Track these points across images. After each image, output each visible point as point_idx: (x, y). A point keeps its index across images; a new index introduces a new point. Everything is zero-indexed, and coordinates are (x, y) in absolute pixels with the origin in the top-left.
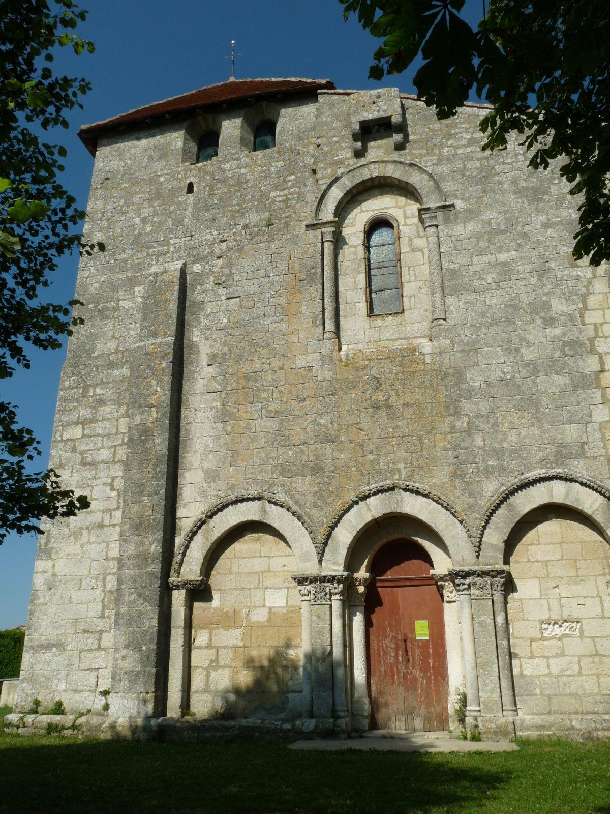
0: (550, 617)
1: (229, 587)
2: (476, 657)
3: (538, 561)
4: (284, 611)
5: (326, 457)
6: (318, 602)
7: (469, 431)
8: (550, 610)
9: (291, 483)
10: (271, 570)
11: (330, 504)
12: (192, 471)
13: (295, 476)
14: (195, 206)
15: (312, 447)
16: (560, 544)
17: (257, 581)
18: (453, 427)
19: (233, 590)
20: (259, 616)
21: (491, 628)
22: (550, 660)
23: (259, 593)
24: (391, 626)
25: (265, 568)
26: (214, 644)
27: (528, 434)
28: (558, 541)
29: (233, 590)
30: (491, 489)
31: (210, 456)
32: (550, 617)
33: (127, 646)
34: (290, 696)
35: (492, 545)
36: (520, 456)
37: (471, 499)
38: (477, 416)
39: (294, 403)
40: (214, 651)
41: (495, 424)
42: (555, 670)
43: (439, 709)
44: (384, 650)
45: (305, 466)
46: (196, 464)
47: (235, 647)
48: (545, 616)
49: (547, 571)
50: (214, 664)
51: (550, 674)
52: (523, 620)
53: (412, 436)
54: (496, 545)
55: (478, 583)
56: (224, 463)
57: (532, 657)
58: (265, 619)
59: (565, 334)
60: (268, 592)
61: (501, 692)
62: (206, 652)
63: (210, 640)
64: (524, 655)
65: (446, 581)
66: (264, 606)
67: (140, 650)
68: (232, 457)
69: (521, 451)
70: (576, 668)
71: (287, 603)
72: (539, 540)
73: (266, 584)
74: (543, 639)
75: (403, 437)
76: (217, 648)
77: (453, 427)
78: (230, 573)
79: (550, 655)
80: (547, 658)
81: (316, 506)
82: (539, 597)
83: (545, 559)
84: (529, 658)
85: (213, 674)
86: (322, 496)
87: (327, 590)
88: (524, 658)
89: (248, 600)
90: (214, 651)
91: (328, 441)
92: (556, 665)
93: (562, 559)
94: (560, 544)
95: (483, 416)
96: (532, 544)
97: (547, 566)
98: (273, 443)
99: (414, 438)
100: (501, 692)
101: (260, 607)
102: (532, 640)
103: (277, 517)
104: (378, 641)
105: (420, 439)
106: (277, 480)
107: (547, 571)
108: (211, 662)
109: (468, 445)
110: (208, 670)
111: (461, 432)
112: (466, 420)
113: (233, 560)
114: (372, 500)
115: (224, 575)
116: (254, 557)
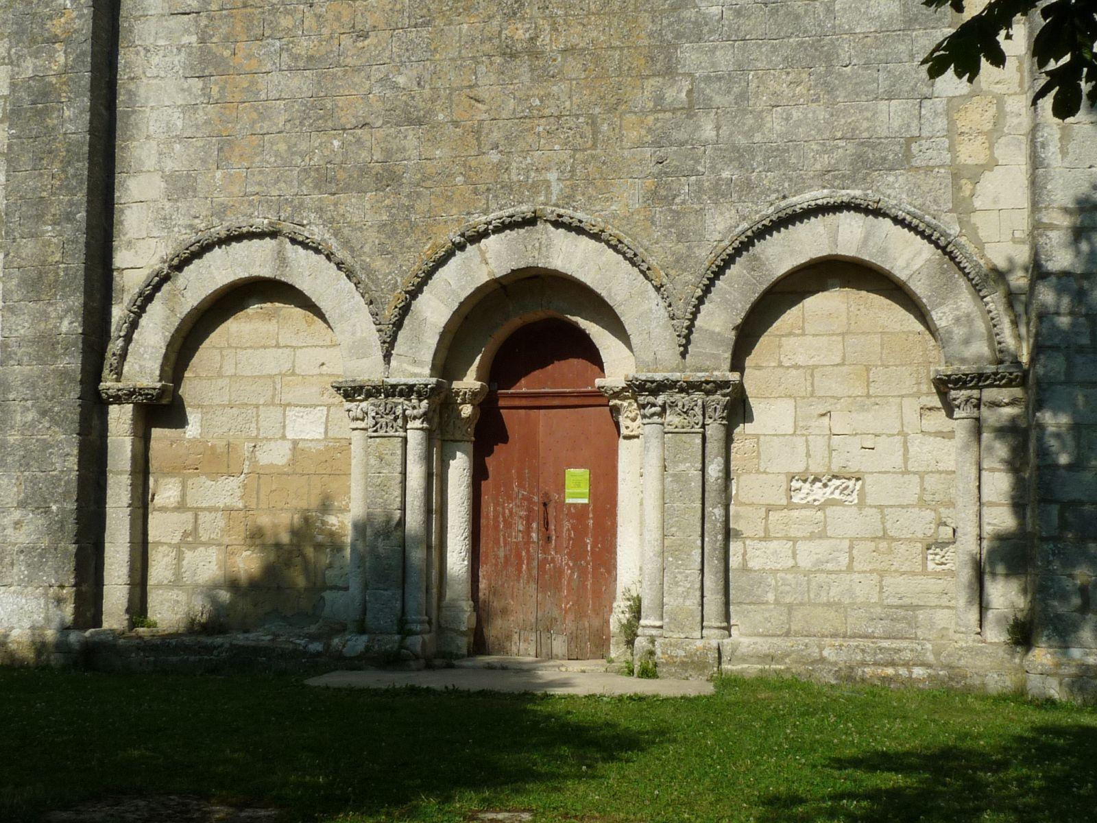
1: (217, 401)
6: (381, 433)
8: (808, 455)
9: (335, 205)
10: (297, 371)
15: (380, 133)
16: (843, 334)
17: (270, 393)
18: (659, 99)
19: (224, 406)
21: (696, 485)
23: (275, 413)
25: (286, 367)
32: (807, 469)
33: (22, 505)
37: (680, 246)
38: (708, 79)
39: (346, 41)
40: (189, 516)
41: (743, 96)
42: (805, 562)
44: (505, 521)
45: (364, 170)
47: (229, 510)
48: (799, 467)
49: (812, 385)
50: (190, 539)
52: (758, 471)
53: (577, 116)
54: (719, 334)
56: (204, 161)
57: (766, 538)
60: (291, 413)
62: (175, 516)
63: (183, 495)
66: (284, 437)
67: (47, 511)
70: (844, 560)
72: (803, 328)
73: (286, 398)
74: (790, 506)
75: (559, 117)
76: (196, 511)
77: (659, 99)
78: (220, 376)
79: (799, 535)
80: (794, 540)
81: (383, 251)
82: (791, 432)
84: (760, 540)
85: (188, 555)
86: (395, 232)
87: (399, 411)
88: (752, 539)
89: (254, 425)
90: (189, 516)
92: (808, 554)
93: (842, 364)
95: (720, 79)
96: (790, 334)
97: (812, 375)
99: (581, 120)
103: (305, 271)
104: (497, 504)
107: (812, 385)
108: (185, 534)
109: (686, 136)
111: (674, 111)
112: (686, 85)
115: (210, 378)
116: (265, 347)
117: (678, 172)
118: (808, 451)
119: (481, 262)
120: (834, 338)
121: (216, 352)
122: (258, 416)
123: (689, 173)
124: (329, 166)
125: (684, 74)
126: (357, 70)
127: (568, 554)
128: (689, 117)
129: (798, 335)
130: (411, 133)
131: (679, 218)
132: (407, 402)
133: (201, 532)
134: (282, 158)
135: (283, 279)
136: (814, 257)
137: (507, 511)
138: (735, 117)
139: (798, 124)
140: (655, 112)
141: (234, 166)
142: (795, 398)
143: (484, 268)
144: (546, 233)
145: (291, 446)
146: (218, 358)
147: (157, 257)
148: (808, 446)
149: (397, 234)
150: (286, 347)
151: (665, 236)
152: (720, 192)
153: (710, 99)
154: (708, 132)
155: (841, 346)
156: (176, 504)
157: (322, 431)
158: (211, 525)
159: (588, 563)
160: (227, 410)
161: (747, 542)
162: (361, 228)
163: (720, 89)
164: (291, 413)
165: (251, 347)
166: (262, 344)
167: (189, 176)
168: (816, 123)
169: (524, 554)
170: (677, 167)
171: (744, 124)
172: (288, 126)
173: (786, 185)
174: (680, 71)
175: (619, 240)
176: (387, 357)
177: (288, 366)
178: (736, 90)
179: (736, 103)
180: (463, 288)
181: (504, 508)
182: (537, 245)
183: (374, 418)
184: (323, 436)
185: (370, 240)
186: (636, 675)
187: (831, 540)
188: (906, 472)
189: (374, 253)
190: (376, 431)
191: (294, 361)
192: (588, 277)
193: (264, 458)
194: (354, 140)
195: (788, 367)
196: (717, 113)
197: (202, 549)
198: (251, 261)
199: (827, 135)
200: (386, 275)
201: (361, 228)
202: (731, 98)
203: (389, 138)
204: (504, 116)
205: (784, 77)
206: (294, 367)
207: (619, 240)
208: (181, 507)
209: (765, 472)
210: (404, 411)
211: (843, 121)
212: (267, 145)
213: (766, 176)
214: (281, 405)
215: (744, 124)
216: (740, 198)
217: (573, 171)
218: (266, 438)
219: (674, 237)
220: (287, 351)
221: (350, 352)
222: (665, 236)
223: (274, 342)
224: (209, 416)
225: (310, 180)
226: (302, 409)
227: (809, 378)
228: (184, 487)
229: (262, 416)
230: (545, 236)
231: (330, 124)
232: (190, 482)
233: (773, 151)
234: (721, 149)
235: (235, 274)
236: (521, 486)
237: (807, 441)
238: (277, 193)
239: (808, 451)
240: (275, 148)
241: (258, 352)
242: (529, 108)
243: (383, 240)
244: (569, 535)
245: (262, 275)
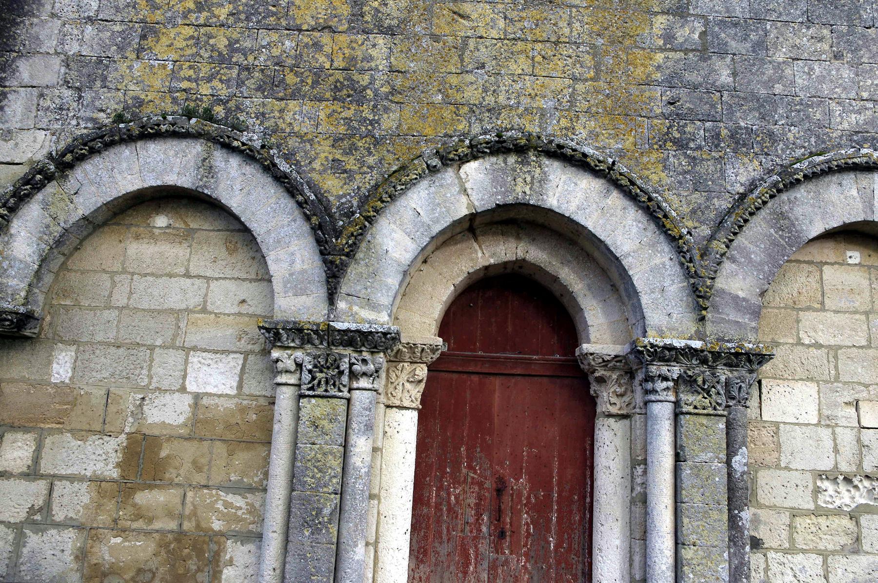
0: (836, 466)
1: (99, 337)
2: (293, 490)
3: (818, 346)
4: (231, 404)
5: (373, 64)
6: (320, 391)
7: (705, 49)
8: (836, 450)
9: (281, 111)
10: (210, 307)
11: (371, 168)
12: (37, 59)
13: (293, 97)
15: (343, 39)
16: (867, 313)
17: (170, 333)
18: (668, 37)
19: (108, 344)
22: (830, 560)
23: (174, 358)
24: (470, 459)
25: (194, 301)
26: (46, 467)
27: (829, 74)
28: (863, 308)
29: (108, 344)
30: (743, 179)
31: (89, 28)
32: (836, 466)
35: (736, 298)
36: (808, 117)
37: (697, 195)
38: (722, 24)
41: (760, 45)
44: (450, 510)
45: (318, 74)
46: (50, 45)
47: (97, 480)
48: (826, 464)
49: (836, 368)
50: (38, 517)
52: (778, 467)
53: (578, 45)
54: (744, 299)
55: (700, 380)
56: (121, 49)
57: (792, 550)
58: (181, 420)
60: (195, 359)
62: (23, 486)
63: (37, 459)
64: (774, 545)
65: (614, 369)
66: (183, 389)
68: (143, 37)
69: (811, 106)
71: (240, 386)
72: (822, 303)
73: (192, 339)
75: (557, 43)
76: (52, 479)
77: (668, 37)
78: (108, 307)
79: (830, 547)
81: (336, 166)
82: (815, 421)
83: (832, 342)
84: (786, 552)
85: (33, 540)
86: (353, 148)
87: (344, 366)
88: (776, 551)
89: (145, 372)
90: (41, 486)
93: (869, 346)
94: (867, 313)
95: (736, 25)
96: (809, 309)
97: (836, 357)
98: (248, 19)
99: (582, 48)
101: (174, 392)
102: (795, 513)
103: (239, 186)
104: (440, 488)
105: (595, 51)
106: (247, 102)
107: (836, 368)
108: (32, 511)
109: (700, 79)
111: (686, 51)
112: (699, 27)
113: (117, 278)
114: (473, 170)
115: (91, 308)
116: (170, 276)
117: (691, 116)
118: (836, 445)
119: (459, 192)
120: (857, 316)
121: (105, 276)
122: (152, 360)
123: (705, 118)
124: (277, 68)
125: (697, 15)
127: (526, 555)
128: (704, 59)
129: (816, 310)
130: (381, 42)
131: (695, 165)
132: (355, 355)
133: (56, 509)
134: (220, 54)
135: (206, 191)
136: (847, 221)
137: (453, 498)
138: (754, 65)
139: (821, 79)
140: (666, 50)
141: (159, 57)
142: (818, 382)
143: (464, 199)
144: (540, 166)
145: (191, 402)
146: (108, 284)
147: (45, 152)
148: (835, 440)
149: (356, 149)
150: (199, 277)
151: (680, 183)
152: (740, 142)
153: (726, 44)
154: (725, 77)
155: (865, 327)
156: (25, 469)
157: (235, 384)
159: (550, 567)
160: (112, 350)
161: (769, 555)
162: (312, 140)
163: (736, 35)
164: (195, 360)
165: (152, 274)
166: (168, 271)
167: (100, 61)
168: (840, 81)
169: (471, 551)
170: (689, 109)
171: (764, 74)
172: (231, 20)
173: (813, 140)
174: (691, 12)
175: (630, 181)
176: (331, 298)
177: (198, 300)
178: (753, 37)
179: (754, 51)
180: (436, 221)
181: (449, 494)
182: (529, 179)
183: (310, 371)
184: (234, 392)
185: (323, 155)
187: (868, 556)
189: (325, 171)
190: (312, 389)
191: (206, 295)
192: (591, 222)
194: (311, 43)
195: (809, 346)
196: (733, 59)
197: (53, 532)
198: (168, 164)
199: (853, 95)
200: (339, 197)
201: (312, 140)
202: (748, 45)
203: (354, 45)
204: (492, 35)
205: (804, 30)
206: (205, 302)
207: (630, 181)
208: (32, 473)
209: (787, 468)
210: (351, 365)
211: (869, 82)
212: (204, 39)
213: (790, 131)
214: (183, 348)
215: (764, 74)
216: (762, 150)
217: (572, 102)
218: (159, 389)
219: (690, 185)
220: (197, 282)
221: (285, 286)
222: (680, 183)
223: (182, 270)
224: (87, 356)
225: (253, 81)
226: (209, 355)
227: (831, 359)
229: (157, 360)
230: (538, 170)
231: (284, 23)
232: (48, 441)
233: (796, 105)
234: (738, 97)
235: (144, 181)
236: (470, 467)
237: (834, 433)
238: (210, 91)
239: (836, 445)
240: (212, 41)
241: (160, 280)
242: (522, 30)
243: (338, 157)
244: (528, 530)
245: (179, 184)
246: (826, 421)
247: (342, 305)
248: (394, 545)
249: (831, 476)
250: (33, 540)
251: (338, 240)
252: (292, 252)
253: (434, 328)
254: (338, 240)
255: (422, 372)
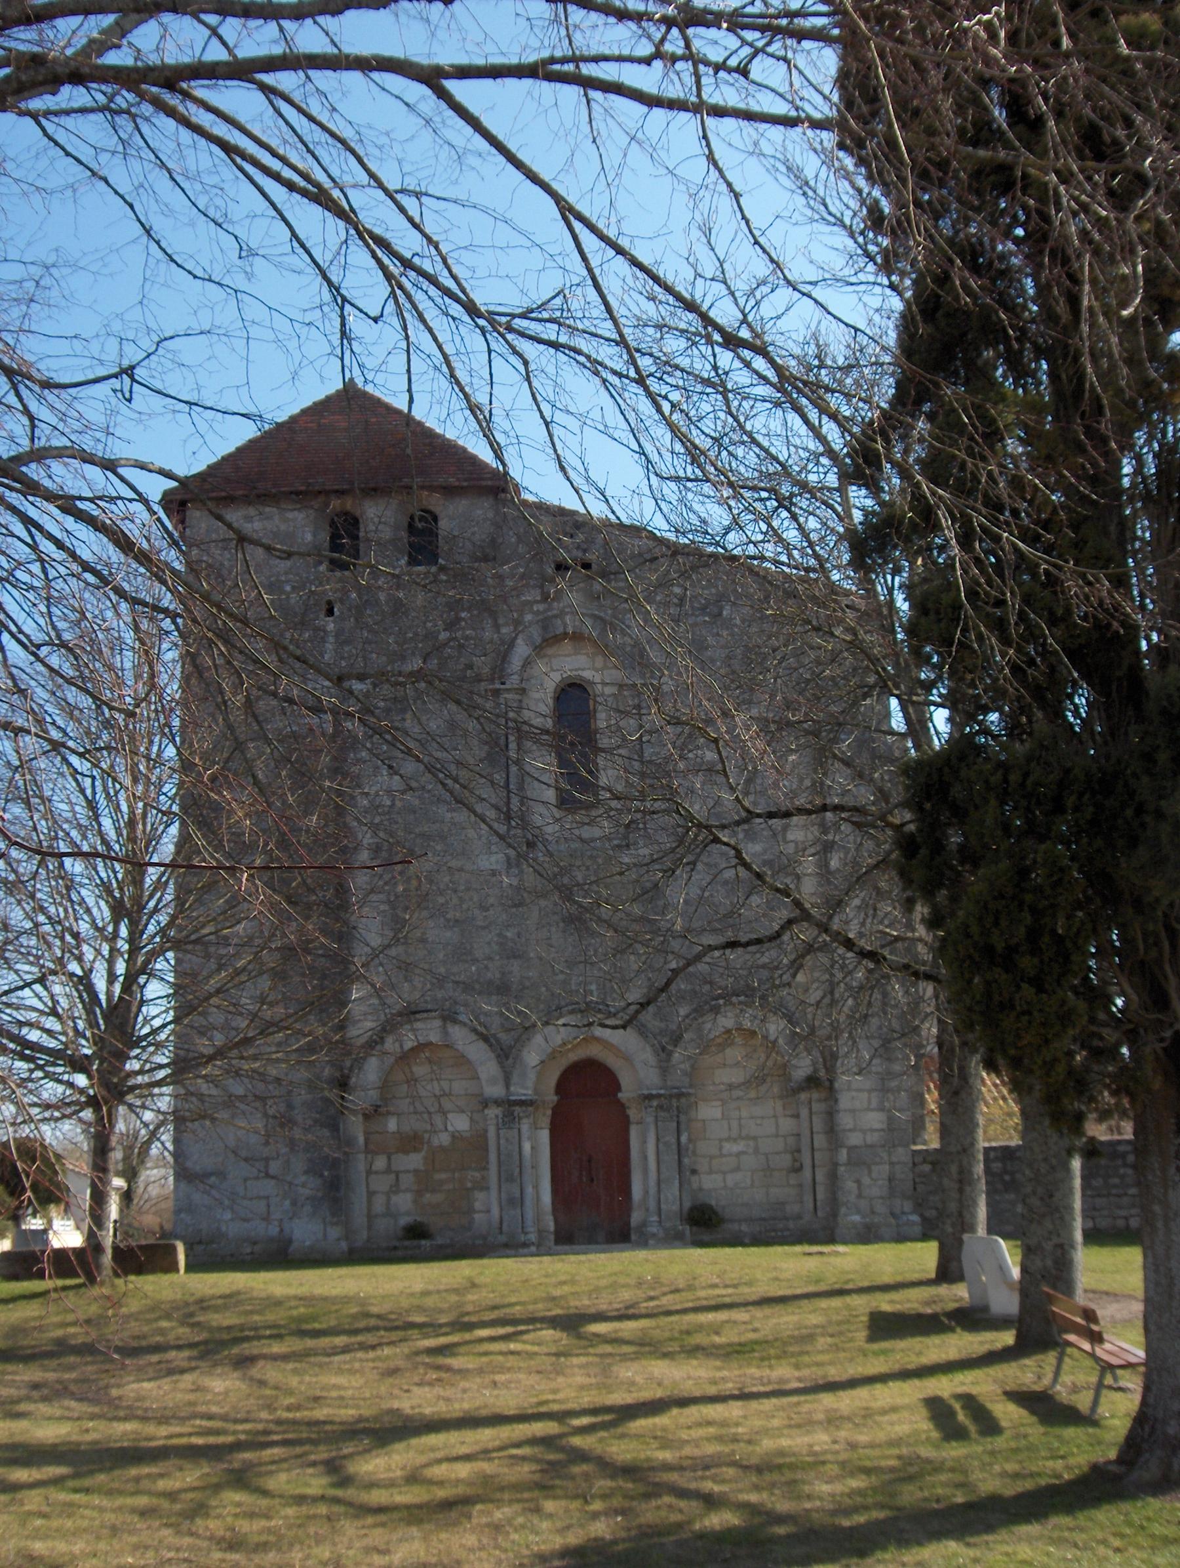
14: (337, 635)
20: (444, 1139)
21: (674, 1147)
26: (394, 1168)
33: (306, 1173)
34: (476, 1216)
39: (477, 912)
40: (393, 1176)
42: (730, 1183)
43: (923, 620)
47: (416, 1171)
51: (725, 1187)
57: (711, 1172)
59: (765, 851)
61: (116, 192)
67: (322, 1176)
70: (749, 1182)
74: (722, 1156)
76: (397, 1173)
80: (724, 1173)
91: (515, 957)
92: (731, 1179)
100: (116, 192)
110: (388, 1195)
126: (484, 928)
158: (407, 1180)
186: (182, 1270)
188: (777, 1136)
193: (436, 1142)
228: (389, 1159)
246: (724, 1117)
247: (512, 1089)
248: (697, 1414)
249: (728, 1139)
250: (394, 1199)
251: (506, 1055)
252: (488, 1067)
253: (552, 1091)
254: (506, 1055)
255: (549, 1112)
